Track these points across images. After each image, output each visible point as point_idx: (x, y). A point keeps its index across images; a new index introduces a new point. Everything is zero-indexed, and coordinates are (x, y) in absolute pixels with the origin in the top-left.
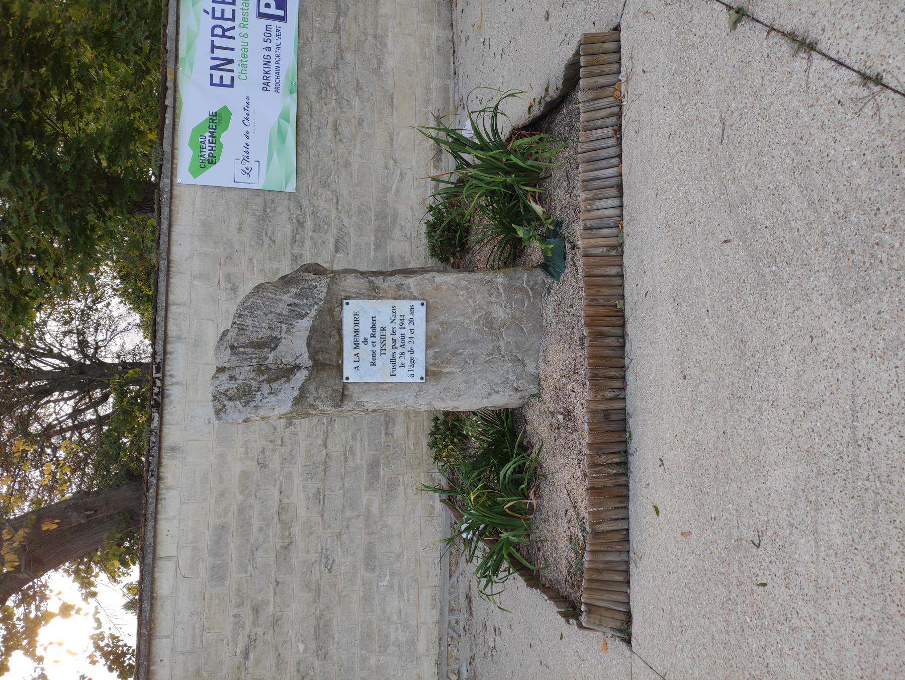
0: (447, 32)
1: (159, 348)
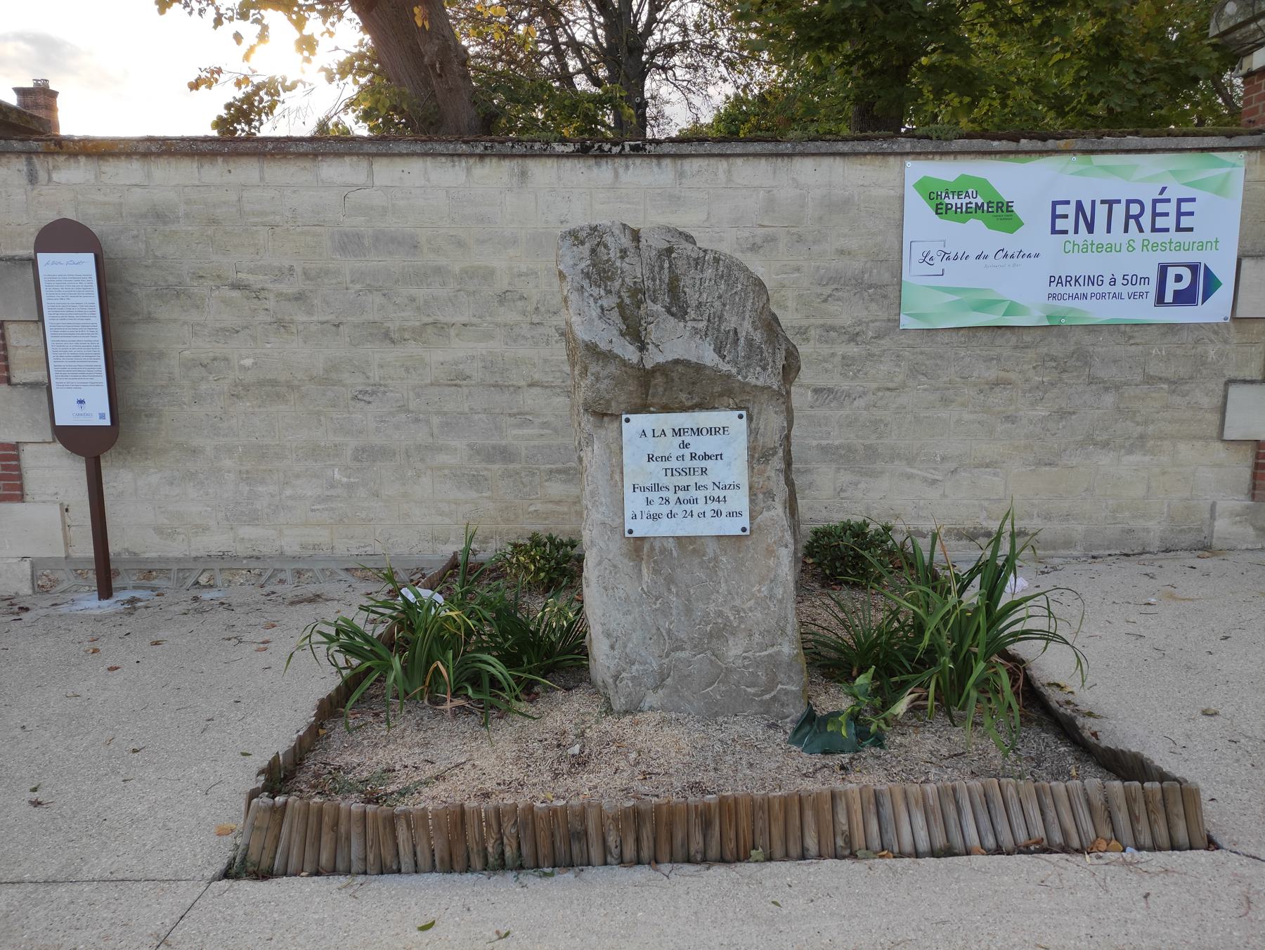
0: (1158, 543)
1: (667, 148)
